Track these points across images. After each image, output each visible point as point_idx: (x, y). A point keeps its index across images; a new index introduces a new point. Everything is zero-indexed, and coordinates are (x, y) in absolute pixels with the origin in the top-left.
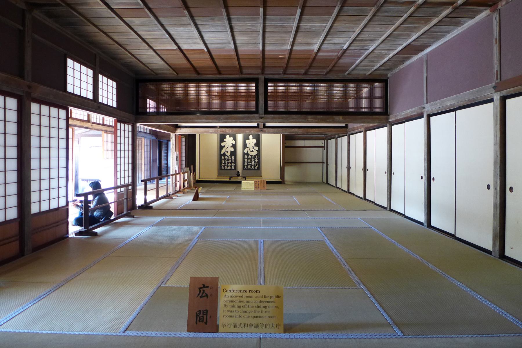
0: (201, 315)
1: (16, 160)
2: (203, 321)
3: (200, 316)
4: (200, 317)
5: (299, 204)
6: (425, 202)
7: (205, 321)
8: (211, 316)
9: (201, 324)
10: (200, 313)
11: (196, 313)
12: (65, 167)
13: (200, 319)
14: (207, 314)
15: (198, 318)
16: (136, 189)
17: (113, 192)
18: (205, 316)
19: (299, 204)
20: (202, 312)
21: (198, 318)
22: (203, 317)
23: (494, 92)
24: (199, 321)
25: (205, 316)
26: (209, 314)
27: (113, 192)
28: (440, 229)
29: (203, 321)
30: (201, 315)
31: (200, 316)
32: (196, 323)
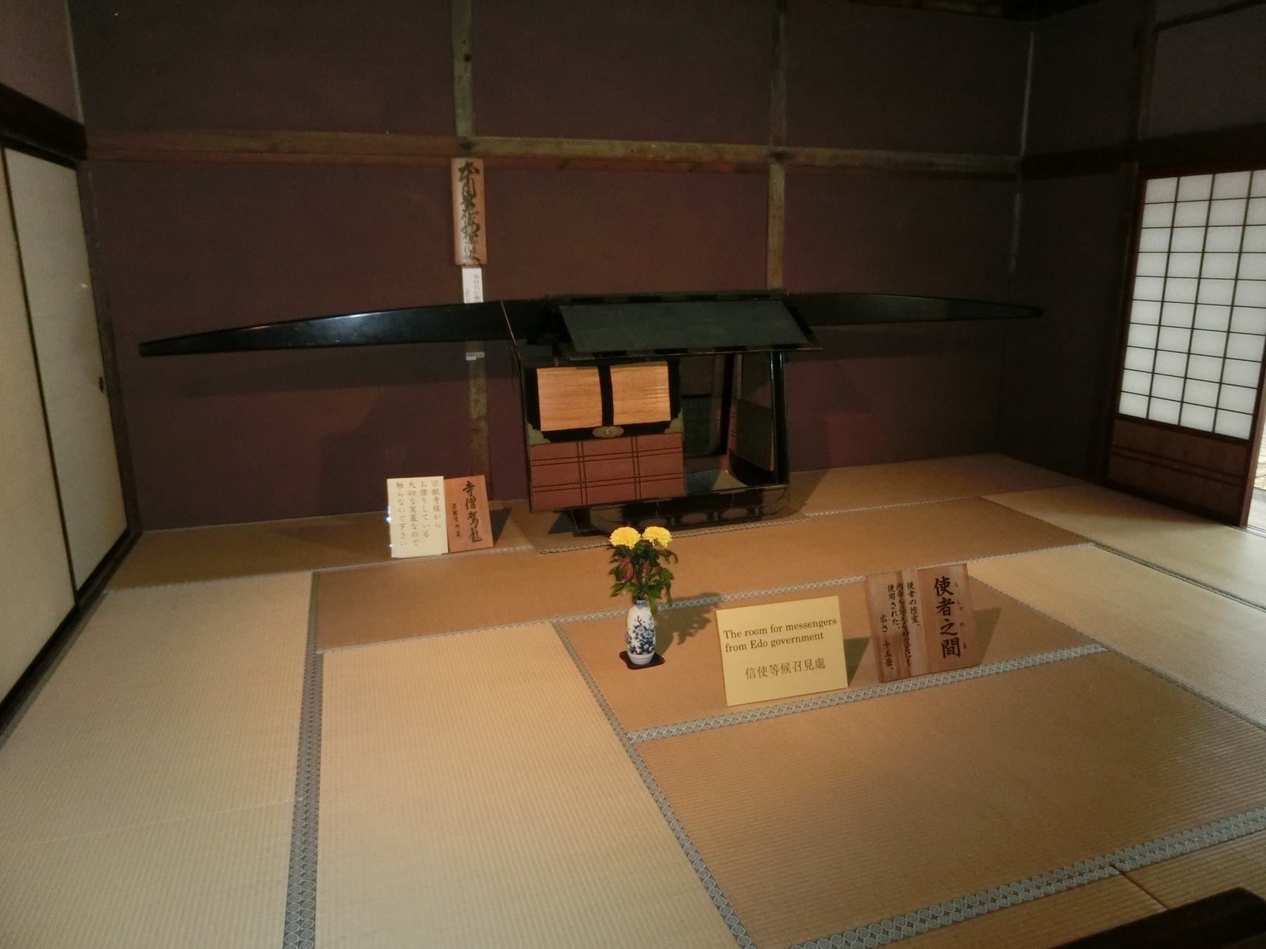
0: (950, 645)
1: (1132, 321)
2: (953, 653)
3: (948, 647)
4: (948, 649)
5: (1018, 197)
6: (44, 684)
7: (957, 652)
8: (965, 645)
9: (952, 658)
10: (948, 644)
11: (942, 644)
12: (1256, 386)
13: (948, 651)
14: (958, 643)
15: (946, 650)
16: (1252, 488)
17: (582, 445)
18: (956, 646)
19: (1018, 197)
20: (950, 641)
21: (946, 650)
22: (953, 648)
23: (593, 514)
24: (949, 654)
25: (956, 646)
26: (961, 643)
27: (582, 445)
28: (1233, 172)
29: (953, 653)
30: (950, 645)
31: (948, 647)
32: (944, 656)
